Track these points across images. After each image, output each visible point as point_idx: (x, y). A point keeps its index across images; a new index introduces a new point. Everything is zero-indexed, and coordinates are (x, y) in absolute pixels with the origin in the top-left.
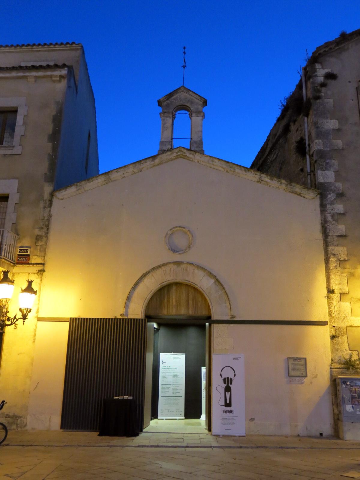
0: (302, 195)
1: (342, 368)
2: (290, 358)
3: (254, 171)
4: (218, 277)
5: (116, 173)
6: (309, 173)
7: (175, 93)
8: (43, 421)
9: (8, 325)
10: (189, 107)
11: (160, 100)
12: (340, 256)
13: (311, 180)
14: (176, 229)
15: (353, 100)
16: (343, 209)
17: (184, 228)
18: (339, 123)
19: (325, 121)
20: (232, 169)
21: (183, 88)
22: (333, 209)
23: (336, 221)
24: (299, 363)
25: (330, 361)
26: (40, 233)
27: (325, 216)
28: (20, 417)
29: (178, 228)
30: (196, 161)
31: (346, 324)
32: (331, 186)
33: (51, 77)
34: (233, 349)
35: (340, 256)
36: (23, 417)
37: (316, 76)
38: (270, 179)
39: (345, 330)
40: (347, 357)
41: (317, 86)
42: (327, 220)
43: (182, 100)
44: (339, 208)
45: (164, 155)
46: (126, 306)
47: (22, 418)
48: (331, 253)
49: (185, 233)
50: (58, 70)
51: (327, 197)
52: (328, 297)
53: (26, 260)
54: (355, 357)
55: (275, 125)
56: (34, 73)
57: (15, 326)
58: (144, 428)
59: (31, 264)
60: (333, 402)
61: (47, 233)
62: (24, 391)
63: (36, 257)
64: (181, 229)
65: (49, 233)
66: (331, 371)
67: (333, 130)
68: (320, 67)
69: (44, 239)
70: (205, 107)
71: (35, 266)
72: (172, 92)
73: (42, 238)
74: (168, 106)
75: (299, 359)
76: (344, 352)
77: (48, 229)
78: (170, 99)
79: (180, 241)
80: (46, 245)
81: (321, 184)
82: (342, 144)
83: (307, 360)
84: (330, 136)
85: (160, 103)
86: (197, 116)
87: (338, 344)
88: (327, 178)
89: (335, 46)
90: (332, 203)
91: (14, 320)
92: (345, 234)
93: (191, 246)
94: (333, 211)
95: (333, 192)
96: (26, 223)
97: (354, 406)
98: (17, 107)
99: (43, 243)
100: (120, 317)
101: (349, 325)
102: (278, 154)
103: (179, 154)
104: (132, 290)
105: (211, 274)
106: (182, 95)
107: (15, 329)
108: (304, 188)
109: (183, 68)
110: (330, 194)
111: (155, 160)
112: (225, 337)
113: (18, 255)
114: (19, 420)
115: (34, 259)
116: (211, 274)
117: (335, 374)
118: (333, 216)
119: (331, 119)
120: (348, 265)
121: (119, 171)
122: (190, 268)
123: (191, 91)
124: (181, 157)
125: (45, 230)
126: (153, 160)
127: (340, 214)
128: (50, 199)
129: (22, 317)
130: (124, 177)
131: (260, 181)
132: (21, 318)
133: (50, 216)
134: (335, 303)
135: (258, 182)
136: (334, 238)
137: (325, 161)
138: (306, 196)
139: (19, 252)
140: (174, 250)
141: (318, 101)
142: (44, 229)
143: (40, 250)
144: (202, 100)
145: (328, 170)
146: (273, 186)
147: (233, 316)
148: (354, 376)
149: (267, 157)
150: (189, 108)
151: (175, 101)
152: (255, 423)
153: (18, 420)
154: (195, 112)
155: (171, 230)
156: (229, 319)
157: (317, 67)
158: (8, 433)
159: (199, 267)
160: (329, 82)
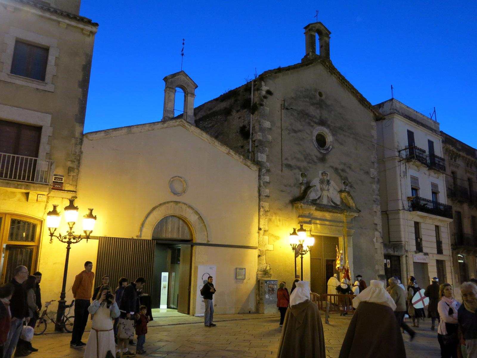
0: (250, 167)
1: (263, 274)
2: (238, 268)
3: (226, 147)
4: (201, 215)
5: (136, 128)
9: (74, 243)
10: (185, 88)
11: (167, 76)
13: (251, 157)
14: (176, 178)
17: (182, 178)
18: (271, 125)
19: (264, 121)
20: (213, 142)
21: (182, 72)
25: (257, 270)
26: (71, 165)
29: (177, 178)
30: (191, 131)
31: (266, 249)
32: (264, 165)
33: (82, 30)
37: (261, 90)
38: (234, 154)
39: (265, 252)
40: (265, 268)
41: (261, 97)
44: (267, 178)
45: (171, 122)
46: (141, 230)
49: (181, 181)
50: (90, 26)
51: (261, 171)
52: (258, 233)
54: (268, 268)
56: (67, 21)
57: (51, 241)
59: (64, 190)
61: (79, 167)
63: (69, 185)
64: (179, 178)
65: (80, 166)
66: (257, 276)
67: (268, 128)
68: (264, 84)
69: (76, 171)
71: (69, 193)
72: (175, 73)
73: (74, 170)
74: (172, 83)
75: (241, 269)
76: (263, 264)
77: (79, 163)
78: (174, 78)
79: (178, 187)
80: (78, 176)
81: (260, 162)
85: (165, 79)
86: (191, 97)
87: (261, 260)
90: (264, 175)
91: (79, 239)
92: (268, 195)
93: (185, 191)
96: (60, 155)
97: (269, 295)
99: (75, 174)
100: (136, 238)
103: (180, 123)
105: (197, 213)
106: (182, 77)
107: (50, 243)
108: (252, 164)
110: (263, 169)
111: (164, 124)
113: (53, 182)
115: (67, 187)
116: (197, 213)
117: (259, 278)
118: (264, 183)
119: (267, 121)
120: (269, 214)
121: (139, 127)
122: (184, 207)
123: (188, 76)
124: (181, 126)
125: (76, 163)
126: (163, 124)
127: (267, 182)
128: (81, 138)
130: (141, 132)
131: (228, 153)
133: (81, 152)
134: (261, 236)
135: (227, 154)
137: (262, 148)
138: (252, 168)
139: (55, 179)
140: (175, 193)
141: (262, 107)
142: (76, 162)
143: (72, 179)
145: (263, 154)
146: (235, 158)
147: (208, 241)
154: (190, 93)
155: (173, 178)
156: (206, 243)
157: (263, 84)
158: (47, 325)
159: (190, 207)
160: (268, 95)
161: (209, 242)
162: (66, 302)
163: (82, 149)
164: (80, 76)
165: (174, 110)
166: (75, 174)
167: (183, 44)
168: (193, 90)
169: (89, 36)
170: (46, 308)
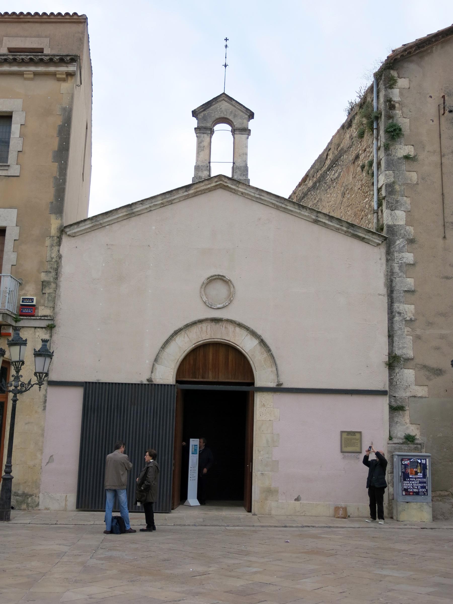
5: (141, 205)
6: (375, 211)
7: (214, 101)
8: (58, 500)
10: (231, 121)
12: (407, 314)
15: (433, 121)
16: (412, 258)
21: (224, 97)
22: (401, 259)
23: (404, 273)
24: (354, 437)
27: (391, 266)
28: (31, 496)
34: (279, 420)
35: (407, 314)
36: (34, 495)
42: (394, 271)
43: (222, 111)
47: (33, 497)
48: (396, 311)
50: (64, 65)
53: (32, 311)
55: (338, 131)
56: (33, 68)
58: (184, 504)
60: (389, 480)
61: (56, 279)
62: (34, 466)
65: (59, 278)
69: (53, 285)
70: (251, 121)
80: (55, 294)
82: (416, 177)
83: (340, 451)
84: (403, 166)
85: (195, 114)
88: (396, 220)
89: (415, 50)
91: (28, 386)
92: (413, 289)
94: (401, 261)
95: (403, 238)
98: (12, 112)
100: (147, 383)
101: (411, 395)
102: (340, 172)
103: (218, 183)
104: (161, 351)
105: (254, 334)
109: (225, 67)
110: (398, 239)
112: (269, 407)
113: (22, 305)
114: (30, 499)
116: (254, 334)
118: (400, 267)
125: (53, 274)
128: (59, 236)
129: (37, 382)
132: (36, 384)
133: (60, 257)
136: (400, 293)
139: (23, 302)
142: (52, 273)
144: (247, 112)
147: (279, 384)
148: (414, 452)
149: (325, 172)
150: (231, 122)
151: (215, 112)
152: (301, 503)
153: (28, 498)
161: (281, 384)
162: (13, 478)
163: (61, 252)
164: (55, 143)
165: (210, 163)
166: (51, 291)
167: (226, 46)
168: (245, 121)
169: (64, 80)
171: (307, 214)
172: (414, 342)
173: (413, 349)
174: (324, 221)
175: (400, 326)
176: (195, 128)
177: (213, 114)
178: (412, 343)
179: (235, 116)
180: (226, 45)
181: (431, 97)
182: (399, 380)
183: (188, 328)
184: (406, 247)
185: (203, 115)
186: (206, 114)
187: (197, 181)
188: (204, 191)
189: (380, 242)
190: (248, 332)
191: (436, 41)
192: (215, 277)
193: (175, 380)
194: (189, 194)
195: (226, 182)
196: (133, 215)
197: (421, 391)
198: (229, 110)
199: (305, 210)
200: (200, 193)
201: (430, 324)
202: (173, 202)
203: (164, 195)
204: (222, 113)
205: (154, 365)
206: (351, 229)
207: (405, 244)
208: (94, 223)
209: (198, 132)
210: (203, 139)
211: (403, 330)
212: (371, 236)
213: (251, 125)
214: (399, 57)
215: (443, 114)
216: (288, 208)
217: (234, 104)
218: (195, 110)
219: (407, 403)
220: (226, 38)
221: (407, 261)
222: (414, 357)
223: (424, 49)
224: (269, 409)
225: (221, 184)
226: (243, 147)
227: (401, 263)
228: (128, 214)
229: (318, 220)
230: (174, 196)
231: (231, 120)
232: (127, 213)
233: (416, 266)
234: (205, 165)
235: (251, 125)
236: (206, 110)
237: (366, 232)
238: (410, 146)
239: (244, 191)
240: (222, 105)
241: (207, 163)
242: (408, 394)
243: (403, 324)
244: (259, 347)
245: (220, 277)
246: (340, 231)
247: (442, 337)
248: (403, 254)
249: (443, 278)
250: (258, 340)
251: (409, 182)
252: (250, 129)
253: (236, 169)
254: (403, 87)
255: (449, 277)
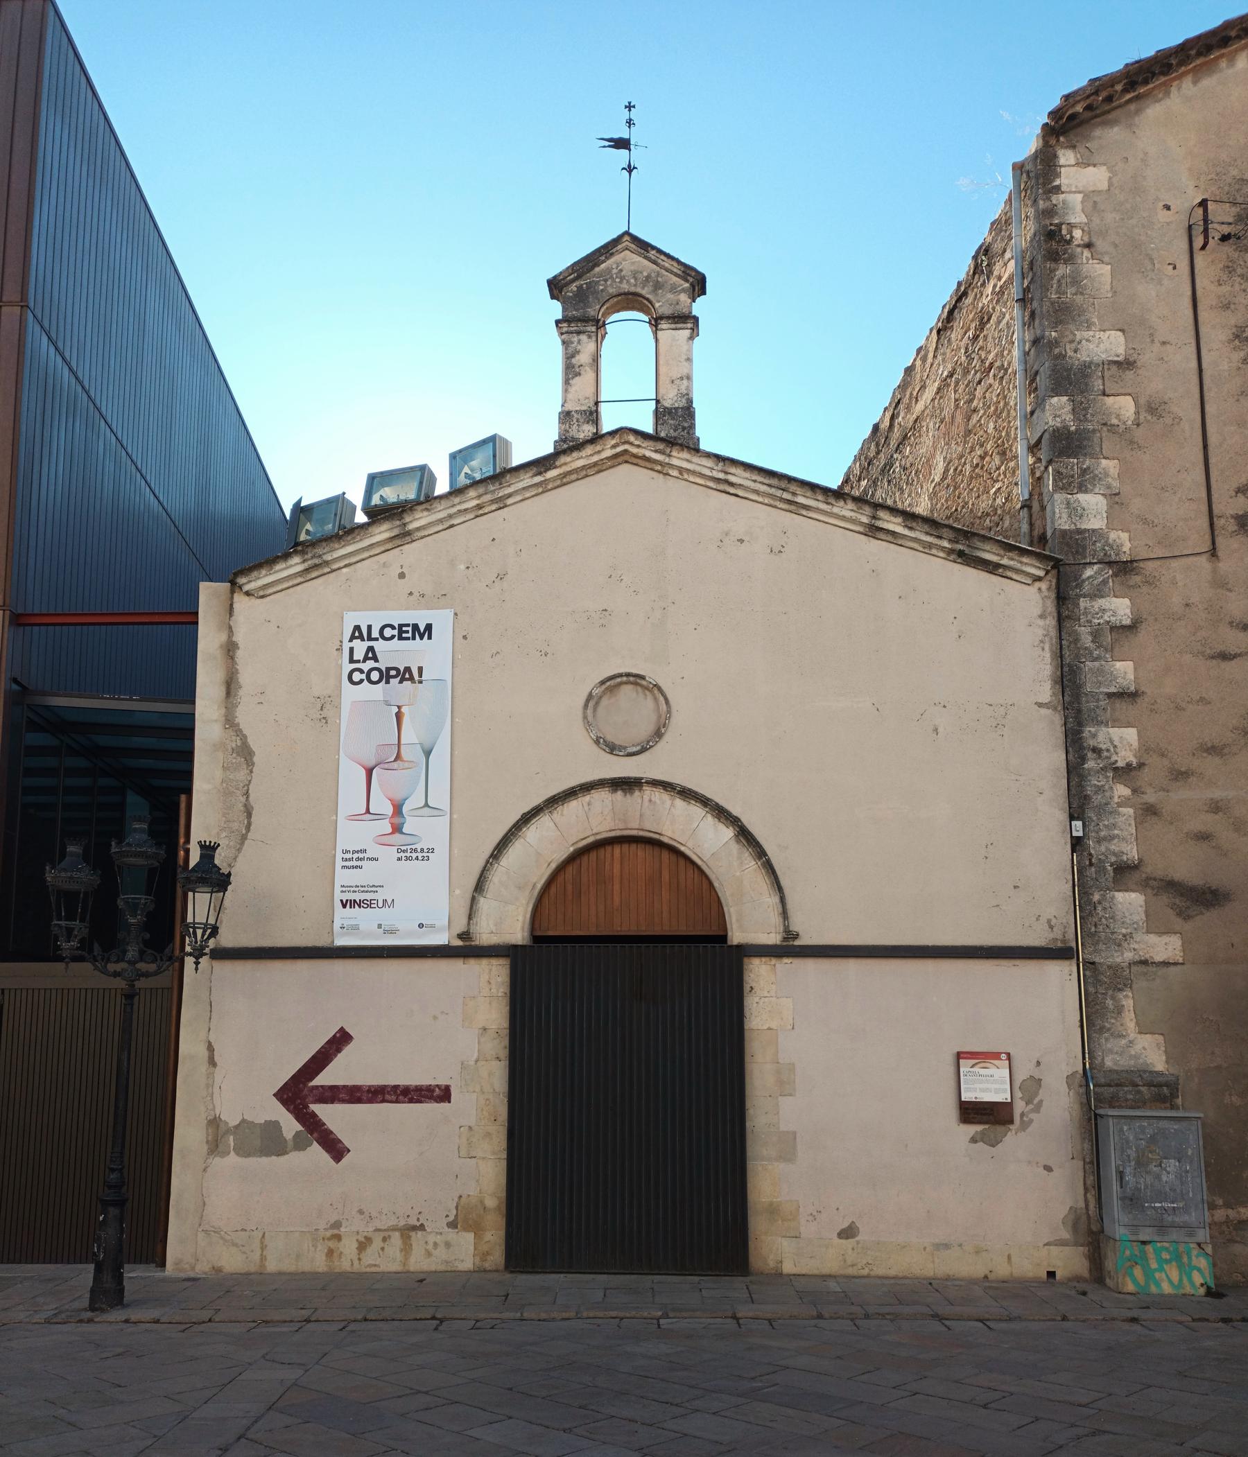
5: (426, 513)
10: (648, 300)
15: (1175, 268)
16: (1128, 611)
34: (793, 1028)
35: (1117, 754)
70: (699, 300)
92: (1132, 689)
101: (1137, 958)
103: (619, 449)
104: (491, 864)
105: (721, 813)
109: (628, 174)
112: (766, 994)
116: (721, 813)
118: (1096, 635)
136: (1098, 700)
151: (606, 281)
159: (687, 794)
161: (796, 936)
165: (597, 403)
170: (1060, 1318)
171: (848, 514)
172: (1139, 823)
173: (1137, 839)
174: (891, 527)
175: (1099, 784)
176: (557, 322)
177: (602, 285)
178: (1134, 824)
179: (658, 286)
180: (630, 120)
181: (1168, 208)
182: (1103, 920)
183: (556, 806)
184: (1111, 584)
185: (575, 289)
186: (585, 286)
187: (567, 446)
188: (584, 473)
189: (1041, 573)
190: (707, 809)
191: (1181, 64)
192: (619, 680)
193: (526, 934)
194: (546, 480)
195: (639, 446)
196: (408, 539)
197: (1165, 947)
198: (641, 273)
199: (842, 503)
200: (574, 477)
201: (1180, 775)
202: (509, 501)
203: (484, 484)
204: (625, 281)
205: (473, 899)
206: (963, 544)
207: (1108, 578)
208: (310, 562)
209: (565, 330)
210: (579, 347)
211: (1107, 794)
212: (1017, 558)
213: (699, 307)
214: (1079, 108)
215: (1203, 248)
216: (800, 500)
217: (653, 257)
218: (555, 277)
219: (1127, 979)
220: (630, 103)
221: (1113, 619)
222: (1140, 860)
223: (1148, 87)
224: (766, 1000)
225: (626, 451)
226: (680, 362)
227: (1099, 624)
228: (395, 536)
229: (877, 527)
230: (509, 486)
231: (647, 296)
232: (393, 535)
233: (1139, 630)
234: (584, 411)
235: (699, 307)
236: (584, 278)
237: (1005, 549)
238: (1113, 332)
239: (685, 465)
240: (624, 263)
241: (592, 404)
242: (1129, 956)
243: (1107, 777)
244: (735, 847)
245: (632, 679)
246: (934, 551)
247: (1216, 807)
248: (1102, 602)
249: (1213, 657)
250: (731, 828)
251: (1115, 421)
252: (697, 315)
253: (664, 416)
254: (1091, 189)
255: (1231, 655)
